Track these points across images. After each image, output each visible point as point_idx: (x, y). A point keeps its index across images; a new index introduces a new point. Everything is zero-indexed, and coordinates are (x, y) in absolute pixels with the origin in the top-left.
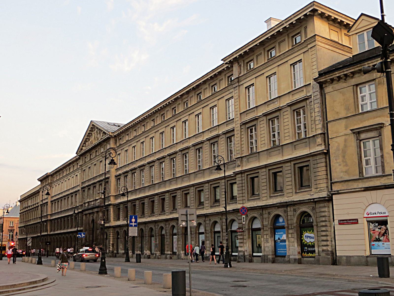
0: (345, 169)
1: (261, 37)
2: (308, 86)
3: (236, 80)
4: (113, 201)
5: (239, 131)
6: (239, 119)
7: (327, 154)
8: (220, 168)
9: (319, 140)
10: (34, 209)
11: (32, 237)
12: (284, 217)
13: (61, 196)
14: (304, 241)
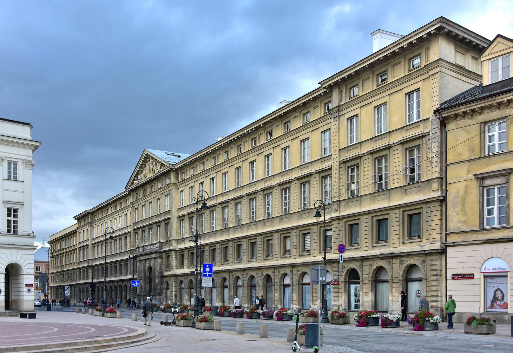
0: (463, 219)
1: (370, 57)
3: (337, 109)
4: (175, 246)
5: (338, 170)
6: (337, 156)
7: (443, 201)
9: (435, 185)
11: (70, 286)
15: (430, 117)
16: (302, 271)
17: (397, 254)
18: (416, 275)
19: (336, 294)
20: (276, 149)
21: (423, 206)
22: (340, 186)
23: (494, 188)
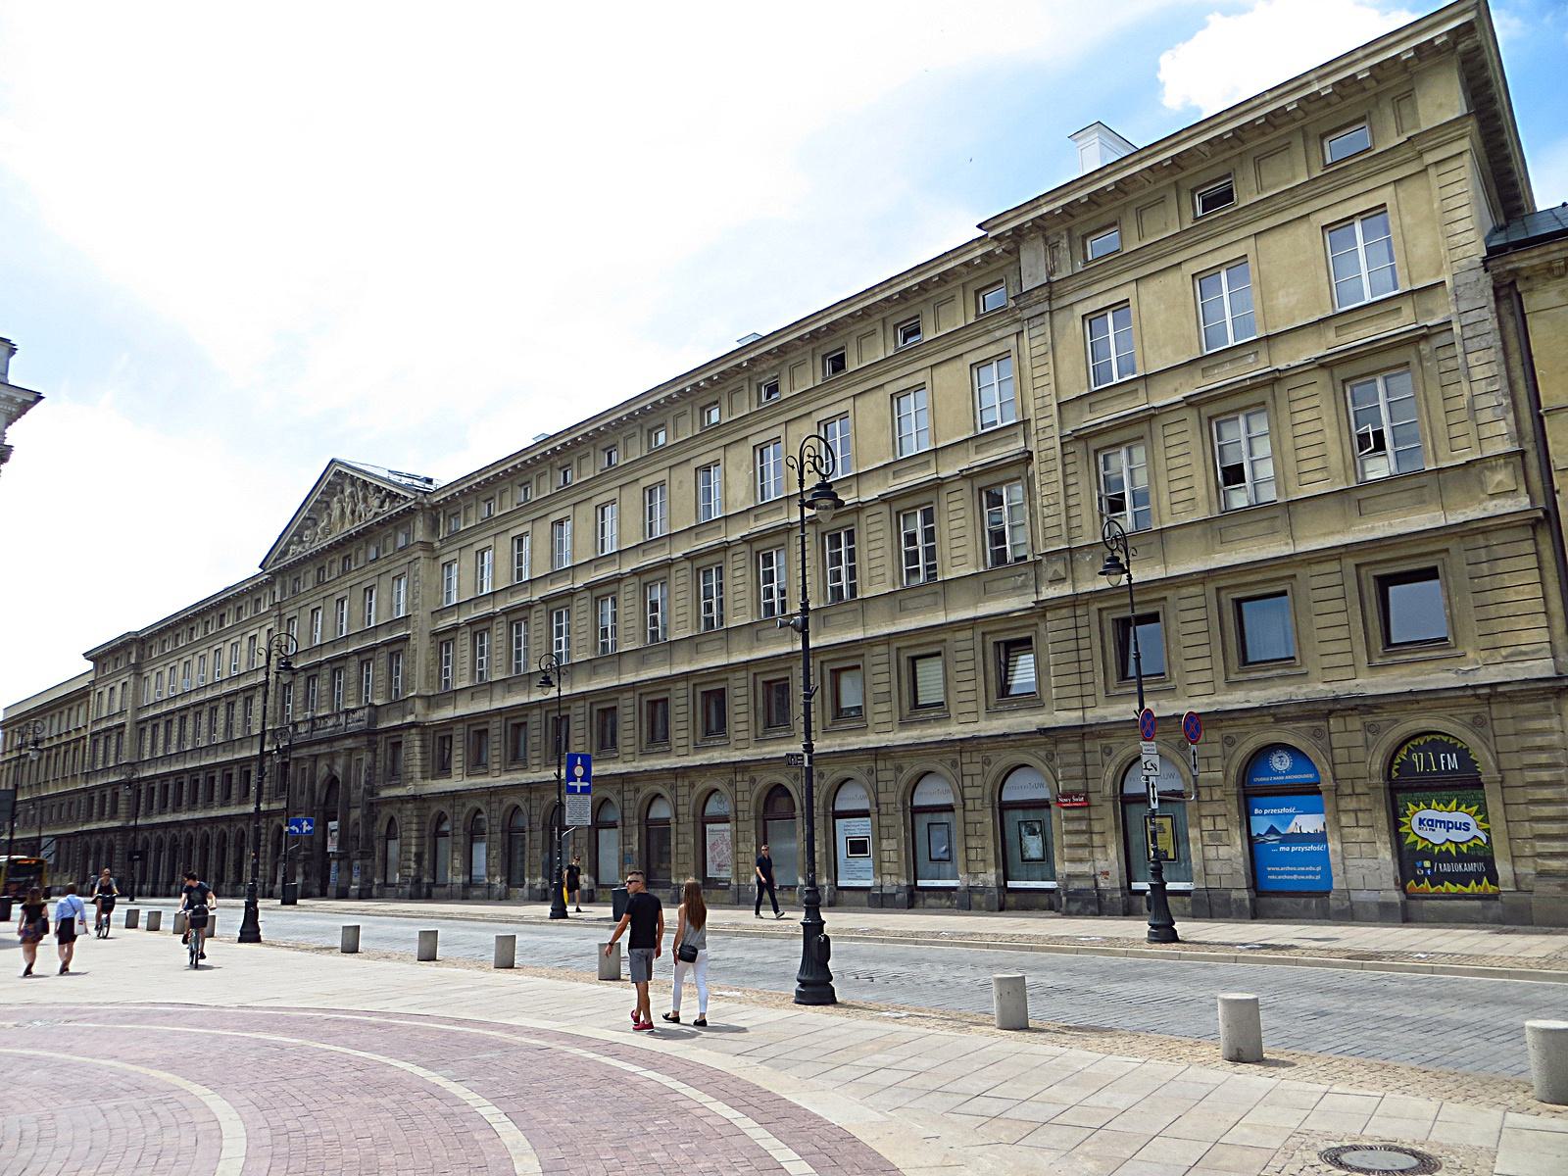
2: (1425, 295)
3: (1045, 291)
4: (418, 713)
8: (551, 683)
10: (54, 751)
11: (56, 837)
14: (1411, 838)
16: (704, 786)
18: (713, 808)
19: (1083, 839)
21: (1451, 544)
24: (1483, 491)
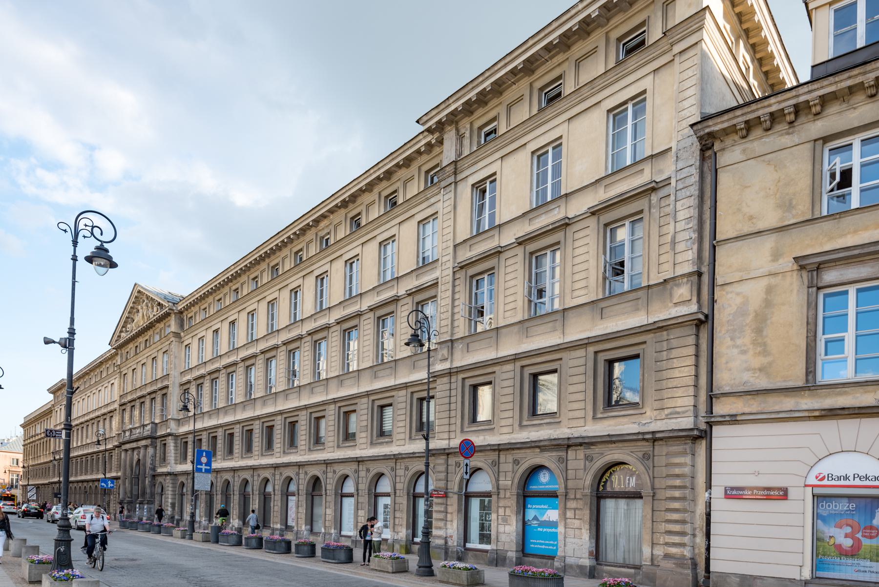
0: (757, 362)
1: (531, 43)
3: (451, 169)
4: (173, 428)
5: (451, 283)
6: (450, 257)
7: (703, 322)
9: (683, 291)
12: (557, 472)
13: (86, 418)
15: (673, 145)
17: (581, 440)
18: (618, 481)
20: (334, 264)
22: (453, 314)
23: (846, 293)
24: (671, 301)
